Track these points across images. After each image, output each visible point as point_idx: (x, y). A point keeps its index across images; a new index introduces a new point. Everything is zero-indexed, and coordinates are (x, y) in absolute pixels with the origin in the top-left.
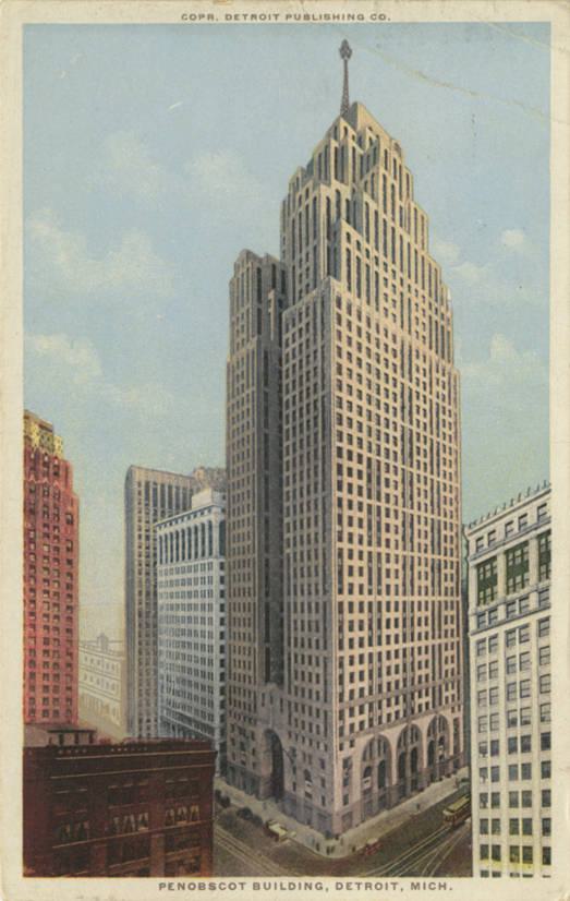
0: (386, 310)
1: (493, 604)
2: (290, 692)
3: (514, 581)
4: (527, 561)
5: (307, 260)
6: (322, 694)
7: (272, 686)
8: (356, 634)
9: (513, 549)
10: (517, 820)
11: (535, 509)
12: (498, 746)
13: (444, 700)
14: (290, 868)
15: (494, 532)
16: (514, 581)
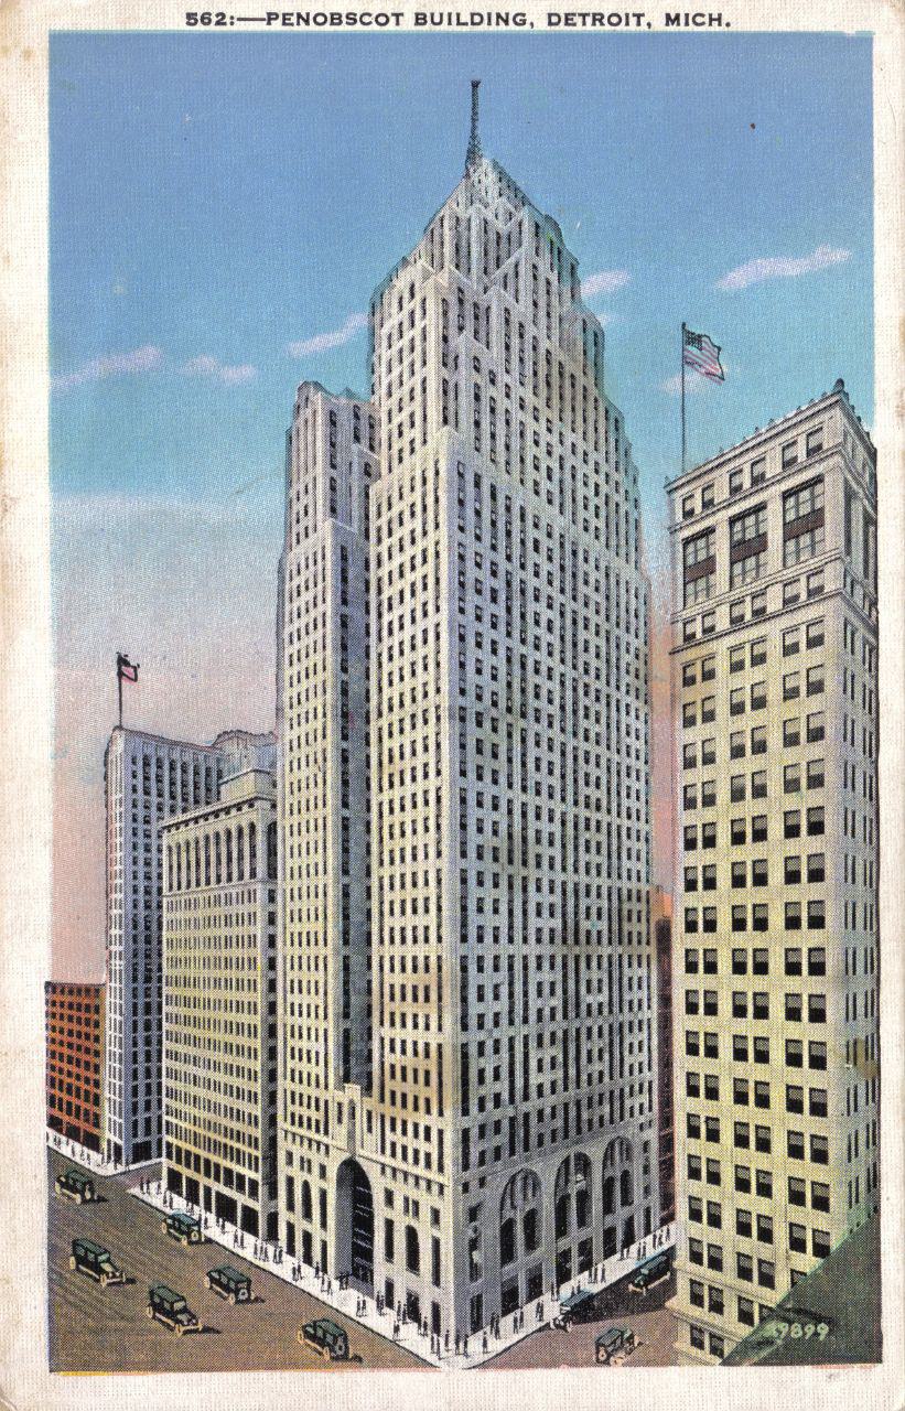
0: (549, 535)
2: (382, 1100)
4: (765, 534)
5: (412, 350)
6: (435, 1157)
7: (353, 1091)
9: (741, 517)
11: (779, 449)
13: (626, 1068)
15: (710, 486)
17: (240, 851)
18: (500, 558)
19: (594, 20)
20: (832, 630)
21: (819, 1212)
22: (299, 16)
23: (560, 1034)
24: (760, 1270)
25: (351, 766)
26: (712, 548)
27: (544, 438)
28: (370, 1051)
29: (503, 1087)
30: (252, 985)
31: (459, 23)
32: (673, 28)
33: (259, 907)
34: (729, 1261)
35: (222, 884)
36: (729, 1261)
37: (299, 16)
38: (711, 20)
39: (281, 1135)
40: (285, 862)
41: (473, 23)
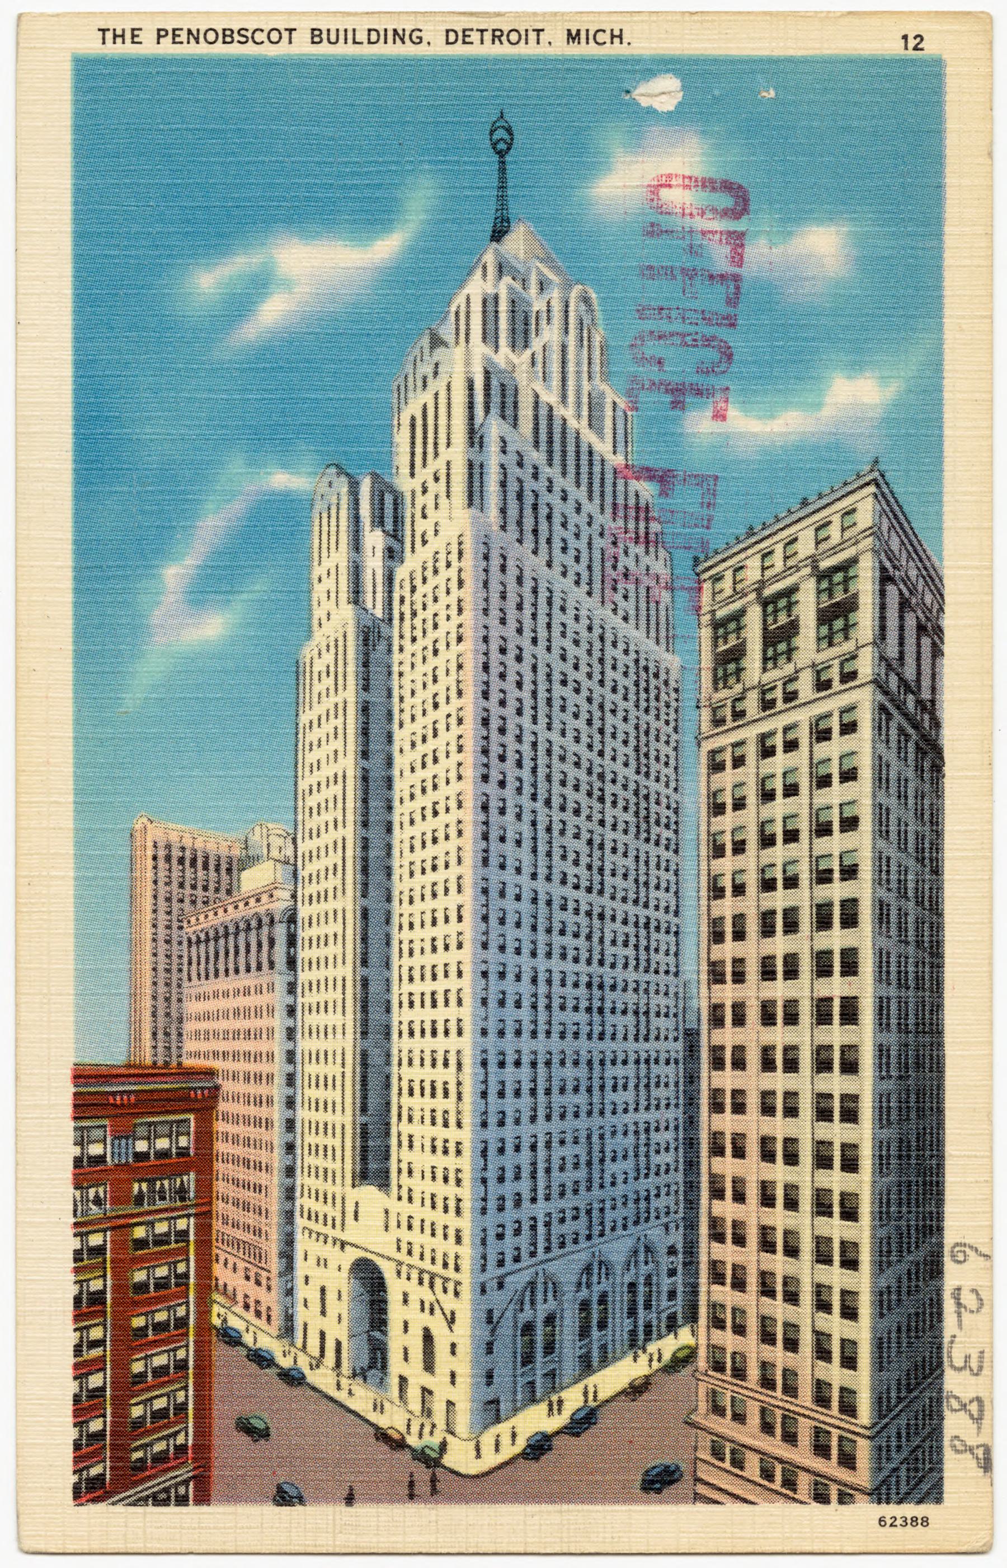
17: (236, 947)
18: (526, 643)
19: (115, 36)
22: (190, 32)
23: (583, 1134)
25: (372, 854)
28: (388, 1147)
29: (524, 1187)
31: (355, 42)
32: (459, 50)
35: (193, 983)
37: (190, 32)
38: (613, 36)
41: (370, 42)
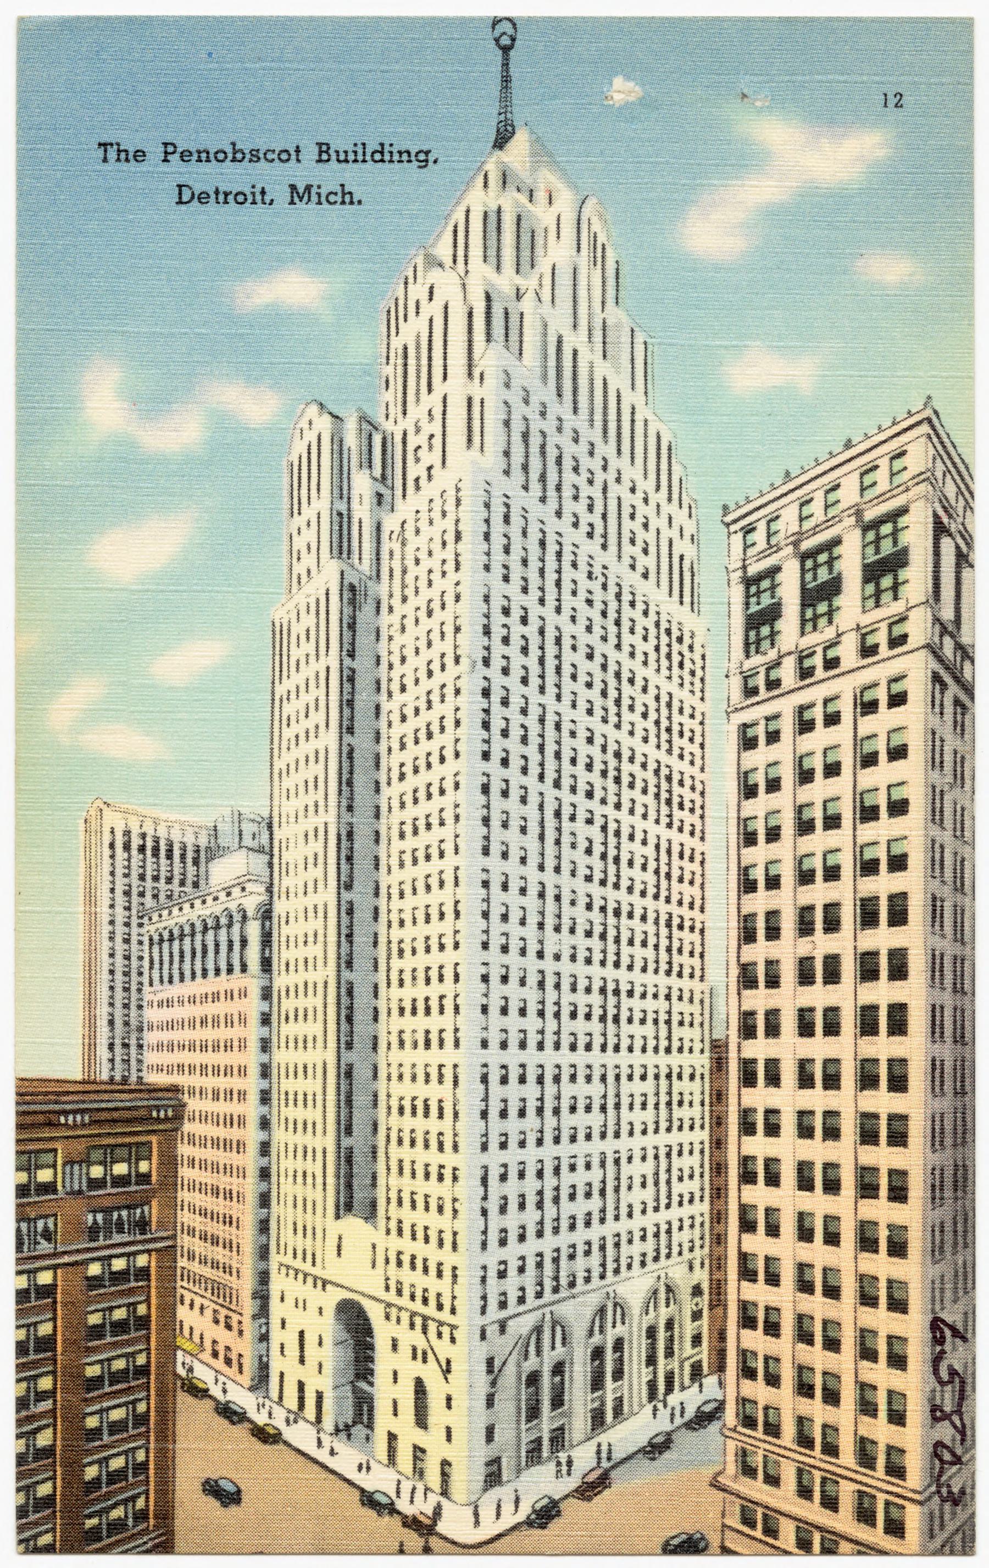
1: (897, 608)
3: (758, 634)
8: (513, 1125)
10: (767, 1035)
12: (778, 921)
14: (832, 122)
16: (758, 634)
20: (917, 797)
21: (894, 1371)
24: (823, 1492)
26: (778, 590)
27: (585, 462)
30: (242, 1071)
33: (253, 1006)
34: (787, 1374)
36: (787, 1374)
39: (273, 1267)
40: (283, 954)
